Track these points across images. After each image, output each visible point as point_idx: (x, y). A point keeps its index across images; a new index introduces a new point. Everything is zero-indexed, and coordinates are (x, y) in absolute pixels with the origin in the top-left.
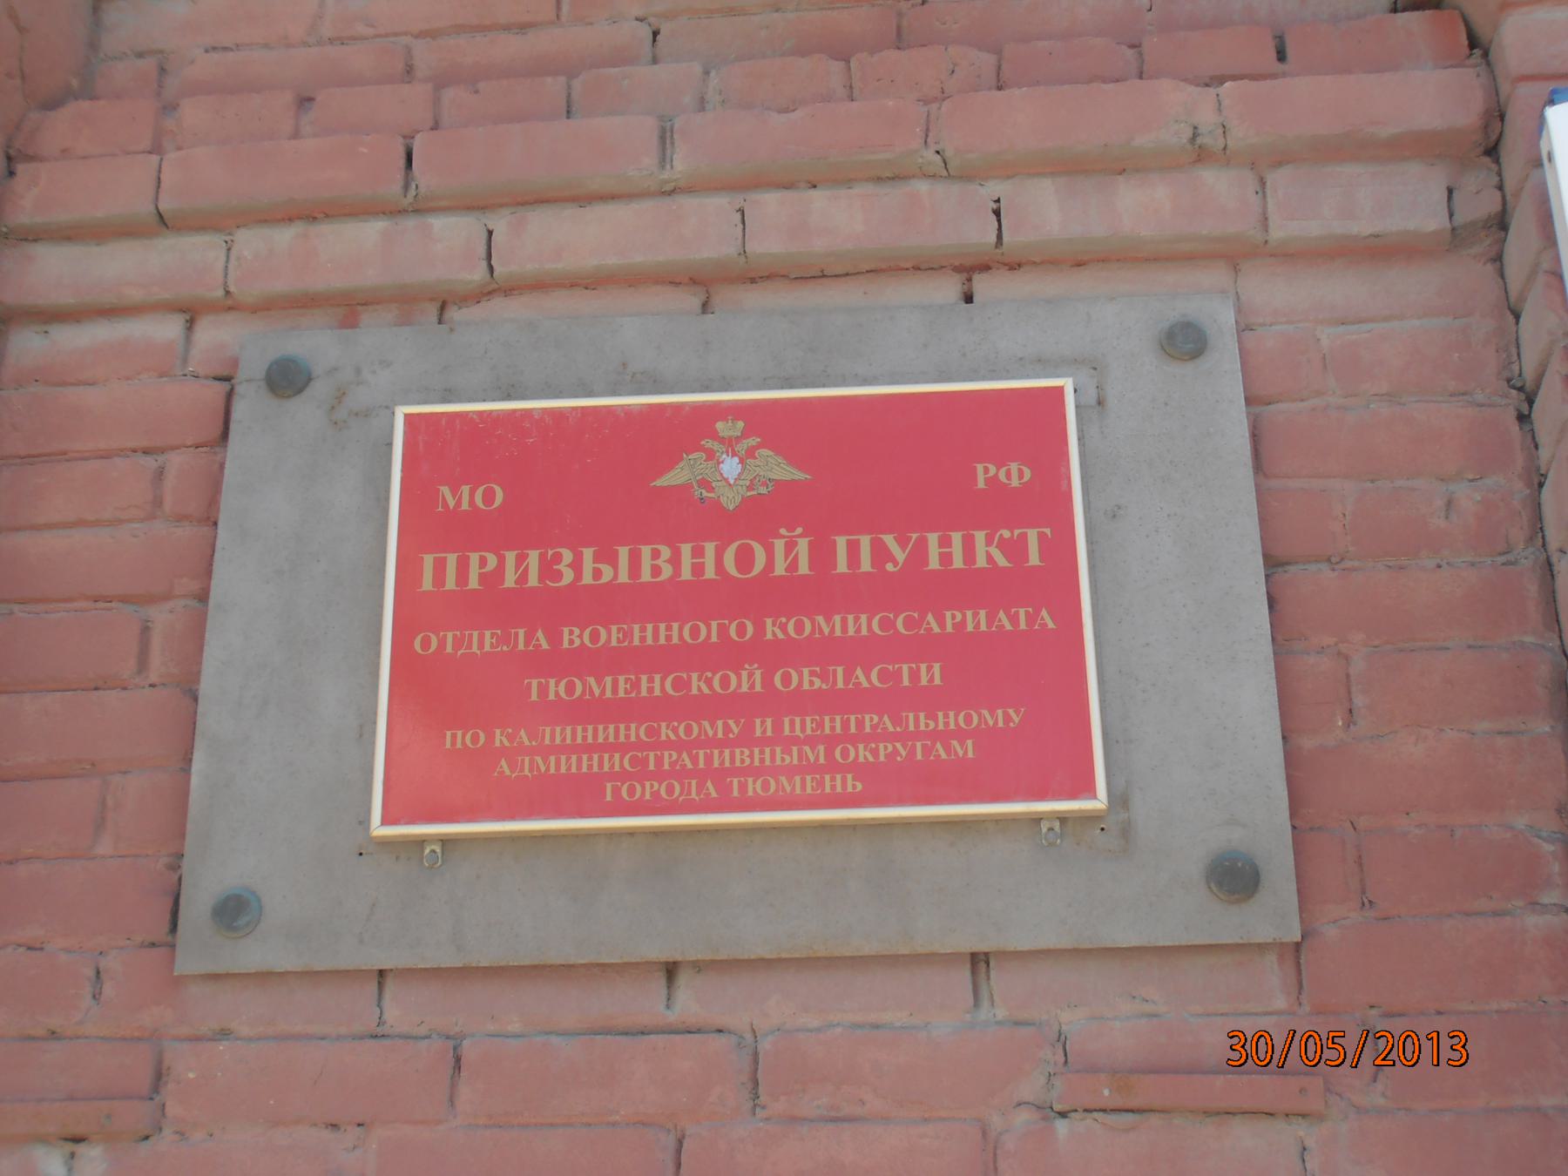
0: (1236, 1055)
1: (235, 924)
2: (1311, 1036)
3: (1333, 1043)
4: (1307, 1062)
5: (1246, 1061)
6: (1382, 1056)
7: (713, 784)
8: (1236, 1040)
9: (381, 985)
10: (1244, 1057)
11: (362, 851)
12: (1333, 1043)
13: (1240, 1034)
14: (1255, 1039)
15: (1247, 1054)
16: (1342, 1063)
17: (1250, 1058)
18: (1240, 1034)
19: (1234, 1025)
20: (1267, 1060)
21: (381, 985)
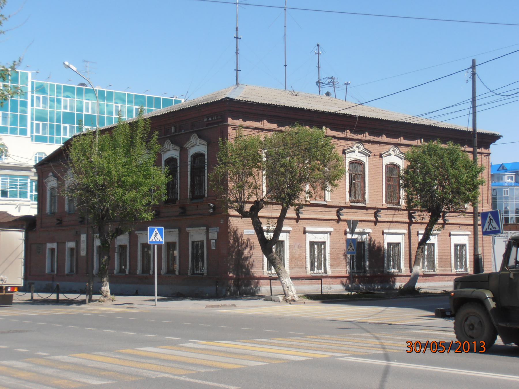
0: (409, 349)
1: (243, 256)
2: (434, 343)
3: (441, 345)
4: (432, 351)
5: (412, 351)
6: (458, 349)
7: (45, 270)
8: (409, 344)
9: (238, 70)
10: (412, 350)
11: (327, 98)
12: (441, 345)
13: (410, 342)
14: (415, 344)
15: (413, 349)
16: (444, 352)
17: (414, 350)
18: (410, 342)
19: (410, 339)
20: (419, 351)
21: (238, 70)
